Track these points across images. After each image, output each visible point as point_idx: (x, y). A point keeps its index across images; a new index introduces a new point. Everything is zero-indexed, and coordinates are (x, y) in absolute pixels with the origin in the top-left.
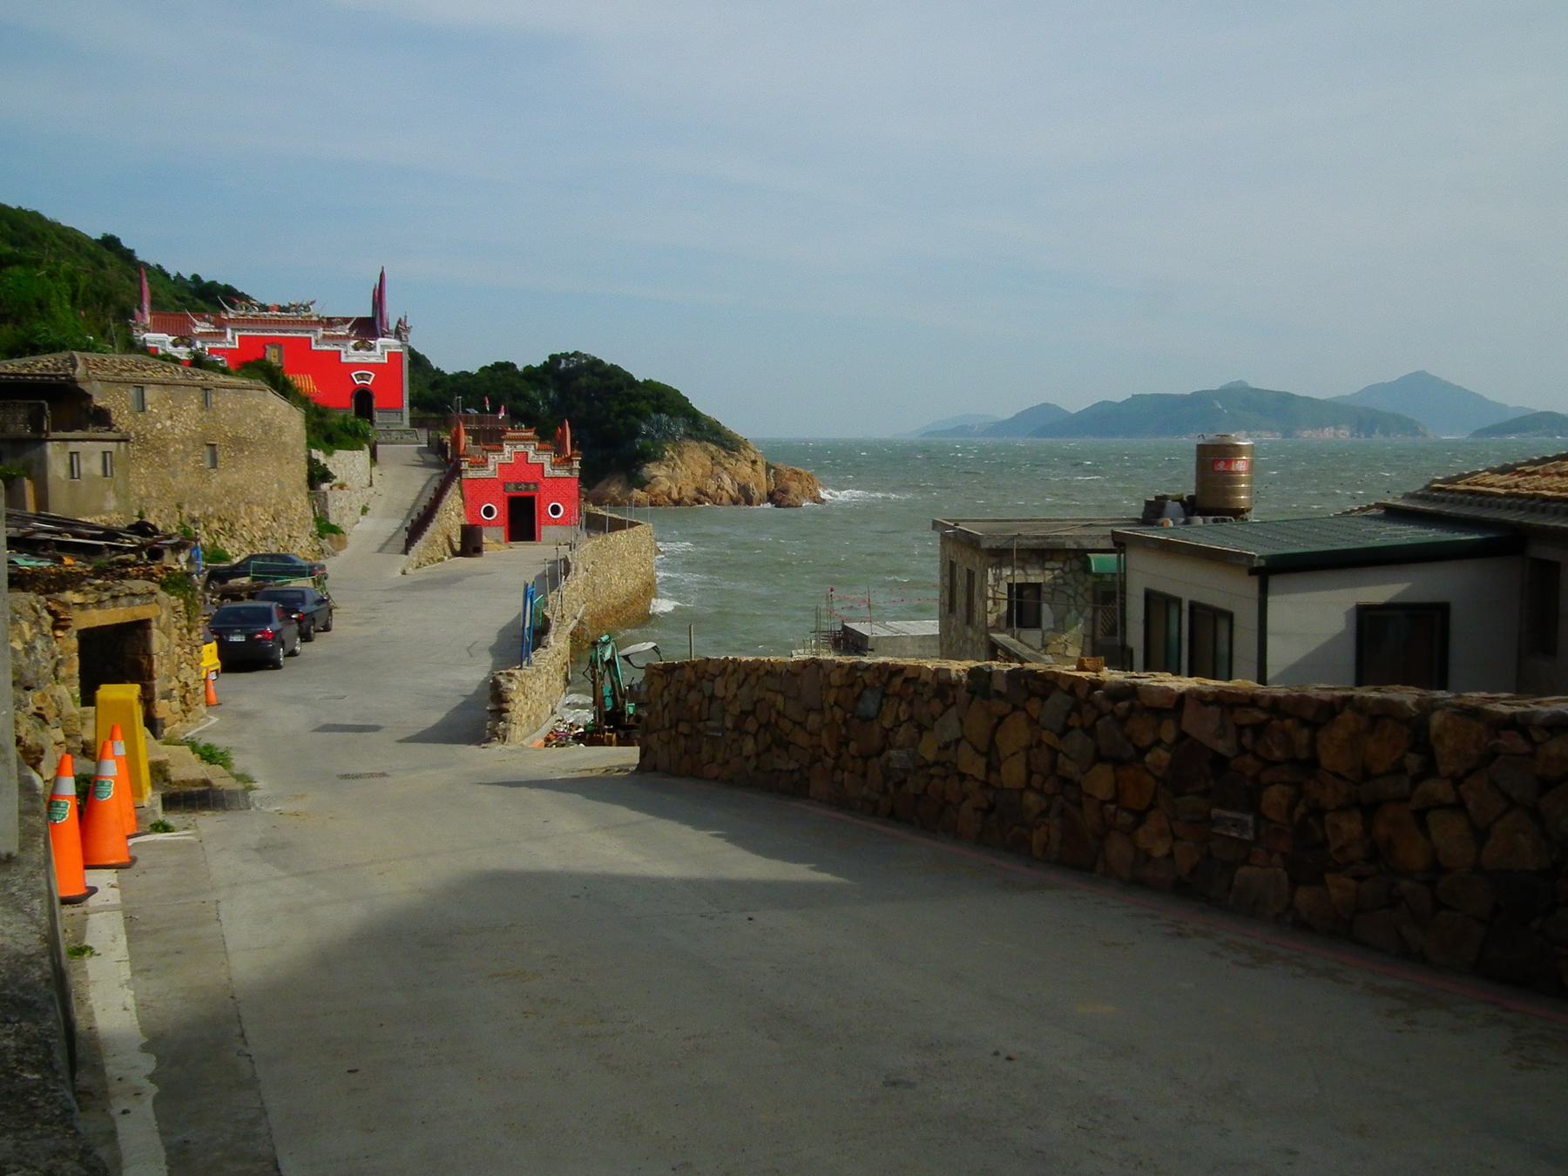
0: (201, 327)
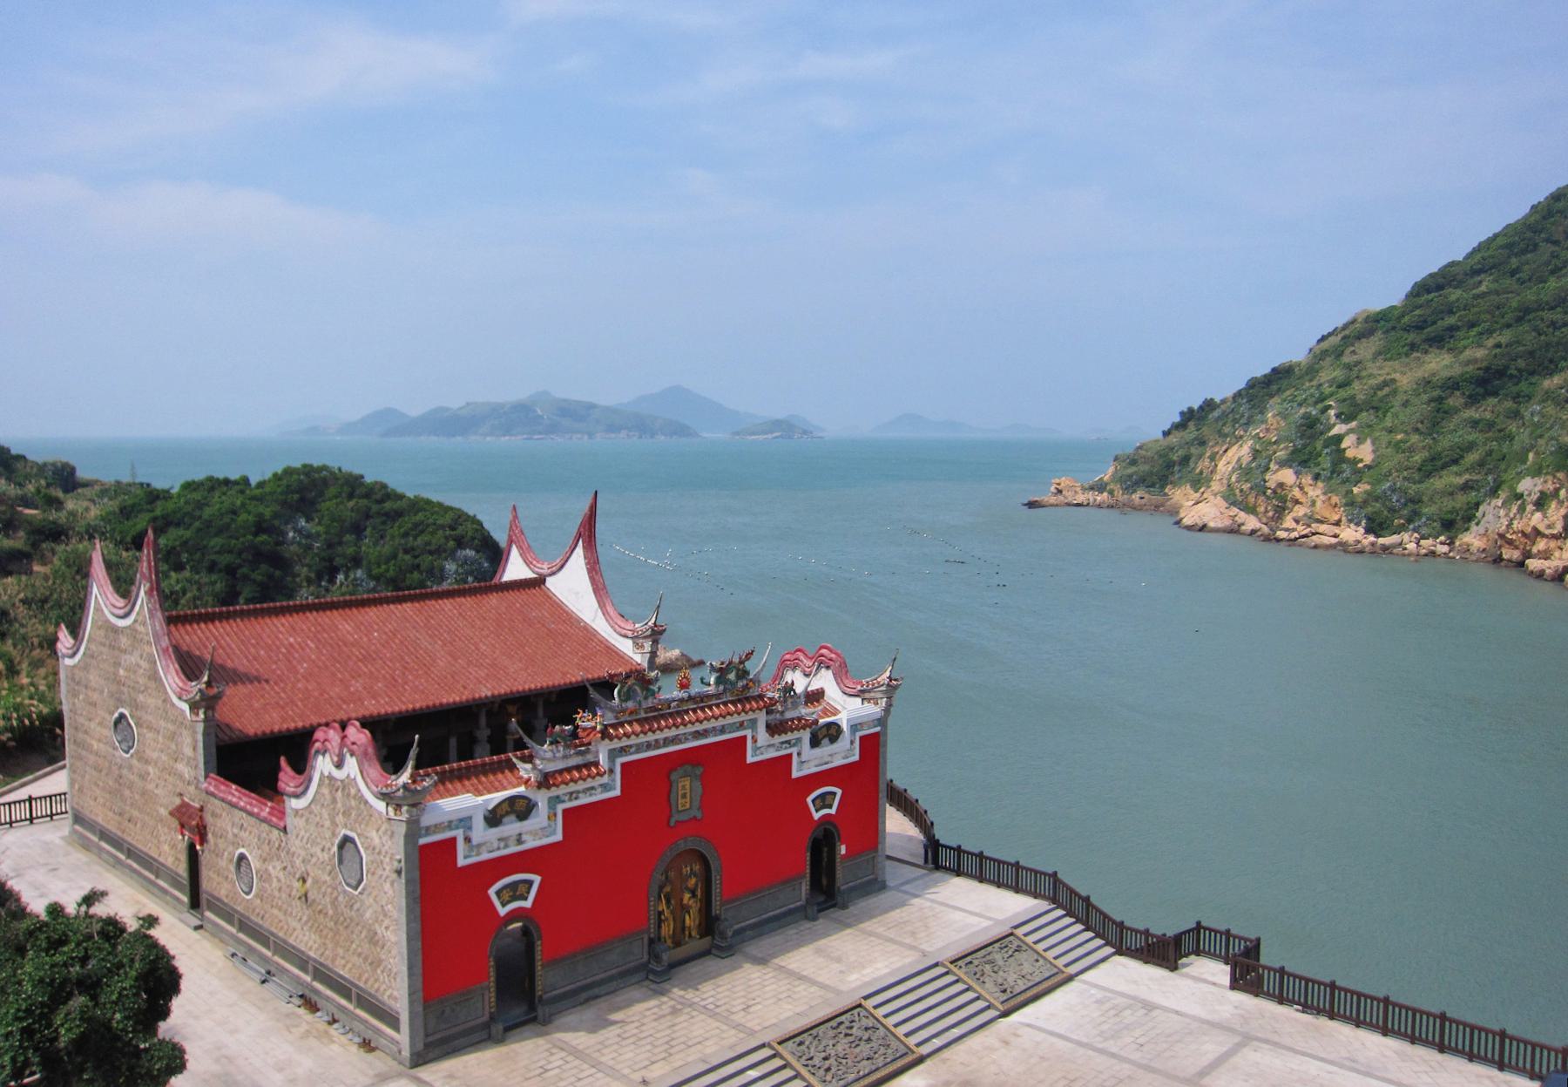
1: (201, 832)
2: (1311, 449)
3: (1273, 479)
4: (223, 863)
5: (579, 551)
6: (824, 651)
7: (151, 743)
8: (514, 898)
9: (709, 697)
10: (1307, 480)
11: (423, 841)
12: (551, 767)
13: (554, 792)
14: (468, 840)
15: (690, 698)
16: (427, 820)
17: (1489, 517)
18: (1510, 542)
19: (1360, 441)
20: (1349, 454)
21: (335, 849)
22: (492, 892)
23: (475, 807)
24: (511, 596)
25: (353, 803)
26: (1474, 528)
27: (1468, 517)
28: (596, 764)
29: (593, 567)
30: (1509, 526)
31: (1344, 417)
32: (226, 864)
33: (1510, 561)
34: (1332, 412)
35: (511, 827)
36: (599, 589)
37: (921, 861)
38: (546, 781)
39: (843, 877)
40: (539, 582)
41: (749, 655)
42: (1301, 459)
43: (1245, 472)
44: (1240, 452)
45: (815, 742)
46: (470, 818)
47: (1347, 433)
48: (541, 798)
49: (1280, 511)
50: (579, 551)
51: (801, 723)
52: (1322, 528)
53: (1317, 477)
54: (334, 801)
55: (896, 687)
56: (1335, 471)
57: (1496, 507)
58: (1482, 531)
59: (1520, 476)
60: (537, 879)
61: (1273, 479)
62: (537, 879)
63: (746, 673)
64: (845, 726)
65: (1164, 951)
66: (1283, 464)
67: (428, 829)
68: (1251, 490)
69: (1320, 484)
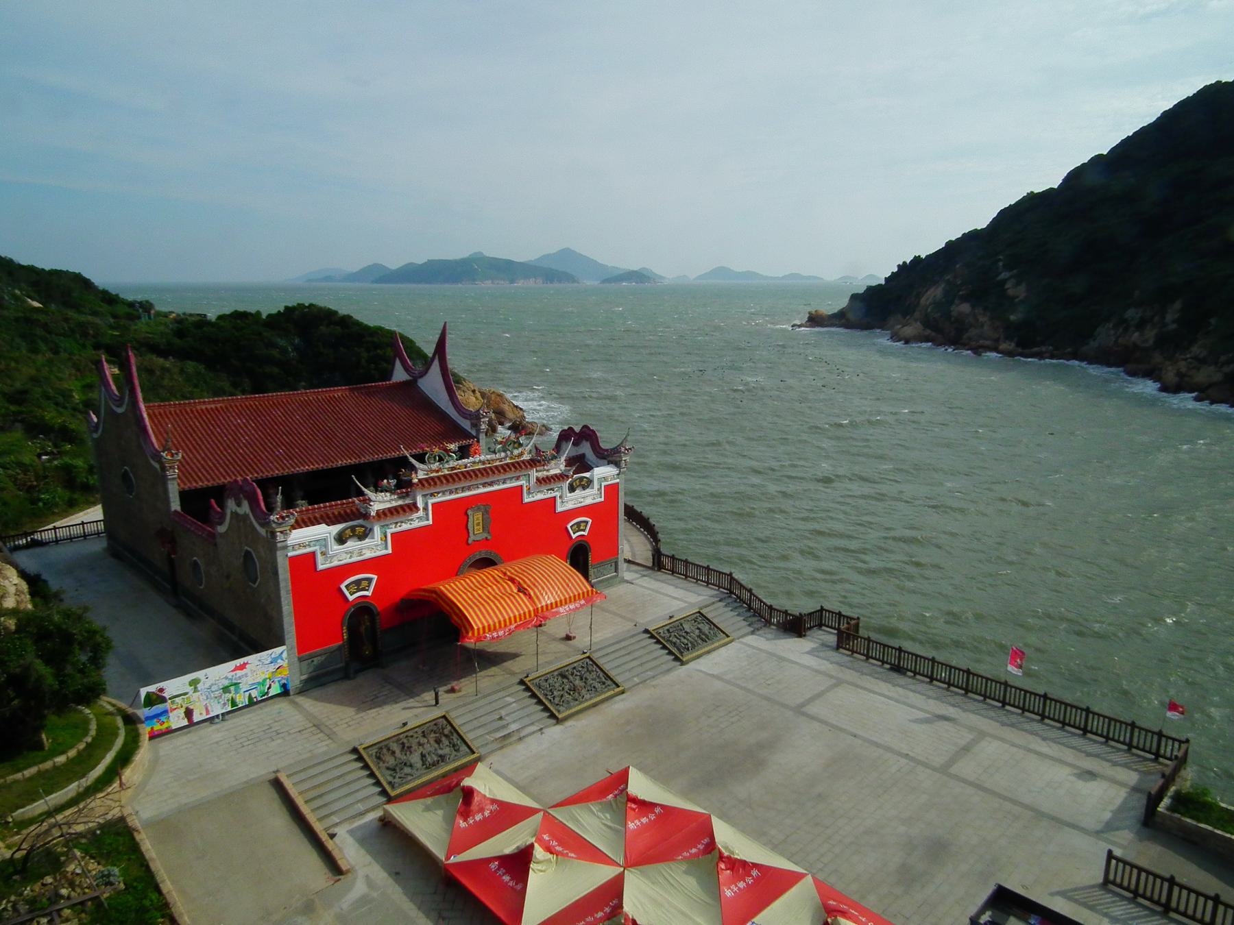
0: (380, 501)
19: (1018, 284)
20: (1011, 292)
34: (1001, 264)
37: (650, 564)
65: (795, 626)
66: (964, 299)
67: (293, 547)
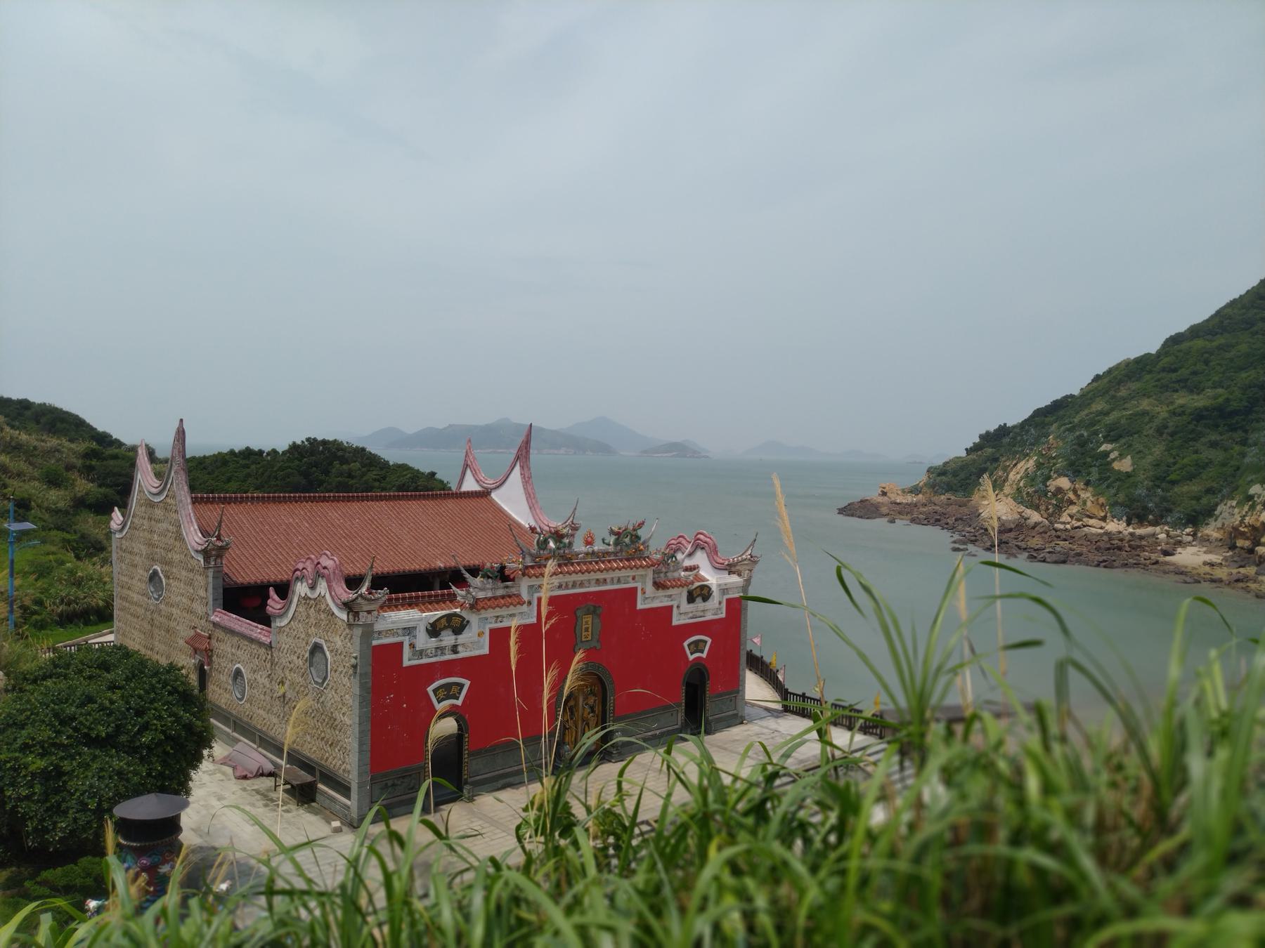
1: (209, 653)
2: (1082, 463)
3: (1053, 485)
4: (223, 678)
5: (517, 468)
6: (701, 537)
7: (177, 591)
8: (448, 697)
9: (608, 553)
10: (1080, 485)
11: (375, 643)
12: (481, 595)
13: (484, 614)
14: (412, 646)
15: (593, 553)
16: (378, 627)
17: (1225, 515)
18: (1243, 534)
19: (1121, 456)
21: (307, 655)
22: (430, 689)
23: (421, 620)
24: (464, 502)
25: (323, 616)
26: (1213, 524)
27: (1209, 513)
28: (518, 596)
29: (527, 480)
30: (1242, 522)
31: (1107, 439)
32: (225, 679)
33: (1242, 548)
35: (448, 639)
36: (530, 497)
38: (475, 606)
39: (712, 708)
40: (484, 494)
41: (641, 525)
42: (1075, 470)
43: (1030, 478)
44: (1029, 464)
45: (691, 599)
46: (415, 628)
47: (1112, 451)
48: (473, 619)
49: (1059, 509)
50: (517, 468)
51: (680, 584)
52: (1091, 522)
53: (1087, 483)
54: (308, 616)
55: (755, 562)
56: (1102, 479)
57: (1232, 507)
58: (1219, 525)
59: (1252, 482)
60: (467, 683)
61: (1053, 485)
62: (467, 683)
63: (638, 538)
64: (714, 588)
67: (380, 633)
68: (1035, 493)
69: (1090, 489)
